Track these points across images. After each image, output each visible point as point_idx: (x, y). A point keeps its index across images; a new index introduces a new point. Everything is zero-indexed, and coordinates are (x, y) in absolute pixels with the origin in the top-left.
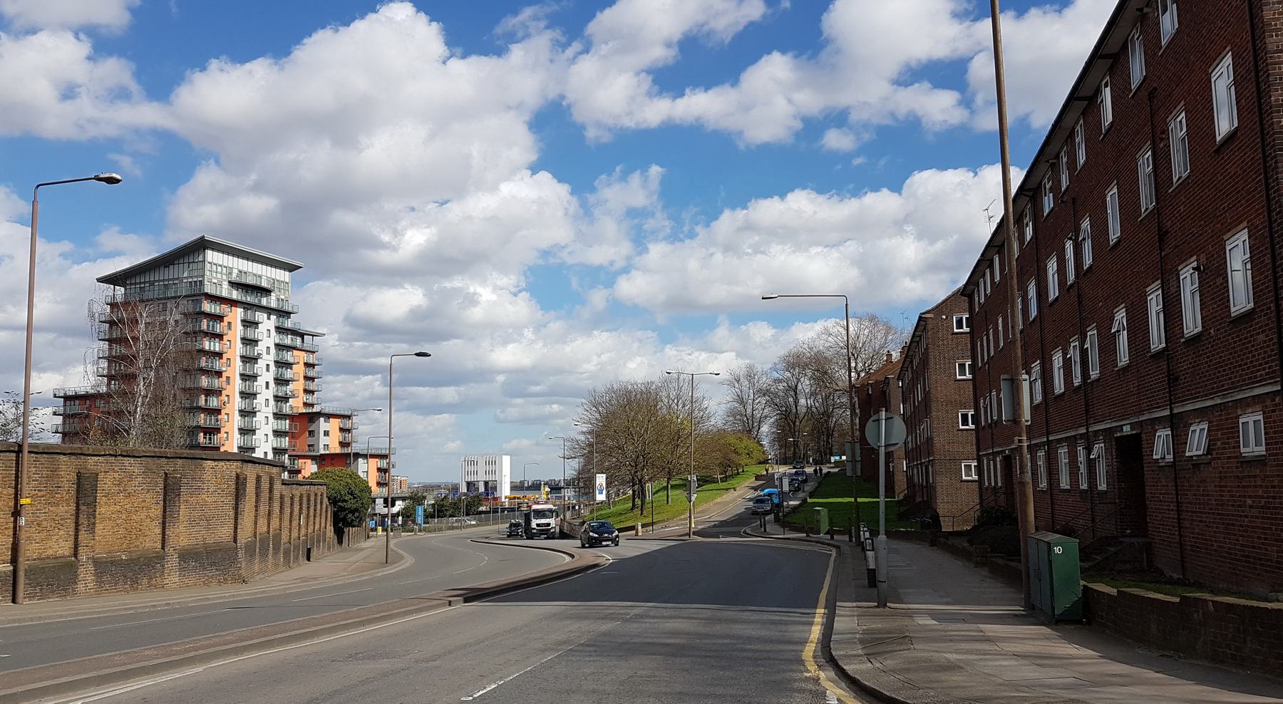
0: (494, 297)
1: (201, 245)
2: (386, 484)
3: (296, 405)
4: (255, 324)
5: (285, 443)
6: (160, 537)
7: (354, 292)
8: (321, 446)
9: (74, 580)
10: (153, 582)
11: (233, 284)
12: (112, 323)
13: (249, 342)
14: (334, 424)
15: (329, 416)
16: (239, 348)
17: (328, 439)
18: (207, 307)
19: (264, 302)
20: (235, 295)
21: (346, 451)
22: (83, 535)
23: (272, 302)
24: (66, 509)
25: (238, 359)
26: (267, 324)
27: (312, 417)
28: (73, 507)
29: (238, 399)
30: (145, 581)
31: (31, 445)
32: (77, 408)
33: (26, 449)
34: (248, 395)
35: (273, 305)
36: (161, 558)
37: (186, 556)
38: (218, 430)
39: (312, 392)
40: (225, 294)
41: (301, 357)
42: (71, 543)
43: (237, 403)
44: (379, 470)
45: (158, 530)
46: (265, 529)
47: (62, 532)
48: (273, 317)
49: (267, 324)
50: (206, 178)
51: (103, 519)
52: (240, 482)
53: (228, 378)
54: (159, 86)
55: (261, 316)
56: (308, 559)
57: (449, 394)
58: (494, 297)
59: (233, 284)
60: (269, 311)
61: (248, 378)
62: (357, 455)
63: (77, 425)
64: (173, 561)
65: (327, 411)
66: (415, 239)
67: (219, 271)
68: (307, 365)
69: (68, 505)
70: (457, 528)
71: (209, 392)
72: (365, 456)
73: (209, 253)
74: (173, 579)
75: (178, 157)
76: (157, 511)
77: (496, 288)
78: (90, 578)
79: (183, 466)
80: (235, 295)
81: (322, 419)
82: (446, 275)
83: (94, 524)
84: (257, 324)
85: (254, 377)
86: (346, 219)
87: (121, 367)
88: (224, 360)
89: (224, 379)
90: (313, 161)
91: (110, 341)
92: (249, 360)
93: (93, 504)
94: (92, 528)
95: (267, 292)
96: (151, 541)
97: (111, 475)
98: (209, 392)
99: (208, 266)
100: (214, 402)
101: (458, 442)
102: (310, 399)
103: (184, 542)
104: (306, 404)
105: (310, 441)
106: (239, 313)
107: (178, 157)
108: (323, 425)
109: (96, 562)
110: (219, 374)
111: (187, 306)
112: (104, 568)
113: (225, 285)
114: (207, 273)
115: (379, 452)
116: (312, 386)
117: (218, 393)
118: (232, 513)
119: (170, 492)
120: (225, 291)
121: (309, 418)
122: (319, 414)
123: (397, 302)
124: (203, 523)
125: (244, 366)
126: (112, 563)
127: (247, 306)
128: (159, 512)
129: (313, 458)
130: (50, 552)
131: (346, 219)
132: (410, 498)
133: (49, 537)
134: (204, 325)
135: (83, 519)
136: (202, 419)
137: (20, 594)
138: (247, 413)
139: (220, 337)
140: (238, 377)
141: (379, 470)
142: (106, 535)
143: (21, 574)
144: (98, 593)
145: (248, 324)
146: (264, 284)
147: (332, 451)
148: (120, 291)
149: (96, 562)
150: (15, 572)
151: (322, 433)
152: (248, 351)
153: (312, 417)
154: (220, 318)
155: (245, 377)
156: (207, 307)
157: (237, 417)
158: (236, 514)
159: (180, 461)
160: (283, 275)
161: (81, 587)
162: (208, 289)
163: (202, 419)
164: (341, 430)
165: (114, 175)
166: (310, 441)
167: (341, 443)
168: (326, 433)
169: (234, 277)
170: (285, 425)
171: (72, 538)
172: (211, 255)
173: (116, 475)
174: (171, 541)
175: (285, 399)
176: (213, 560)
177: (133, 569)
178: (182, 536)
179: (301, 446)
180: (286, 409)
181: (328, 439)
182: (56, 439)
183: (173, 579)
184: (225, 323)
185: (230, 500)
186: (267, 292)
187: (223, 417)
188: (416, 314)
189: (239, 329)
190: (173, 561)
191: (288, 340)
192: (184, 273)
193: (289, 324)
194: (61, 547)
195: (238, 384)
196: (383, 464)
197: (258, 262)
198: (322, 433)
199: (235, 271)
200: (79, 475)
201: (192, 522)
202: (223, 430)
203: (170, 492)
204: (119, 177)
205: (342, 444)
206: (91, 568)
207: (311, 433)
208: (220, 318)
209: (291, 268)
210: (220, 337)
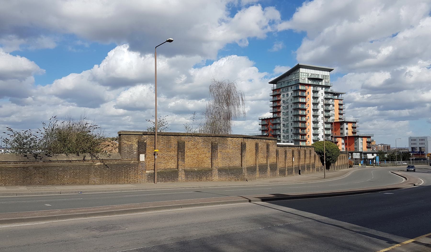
0: (420, 71)
1: (298, 67)
2: (370, 148)
3: (335, 118)
4: (317, 92)
5: (330, 132)
6: (211, 163)
7: (363, 76)
8: (345, 133)
9: (177, 176)
10: (208, 178)
11: (309, 79)
12: (273, 96)
13: (315, 98)
14: (350, 126)
15: (347, 123)
16: (312, 100)
17: (348, 131)
18: (301, 87)
19: (320, 83)
20: (310, 82)
21: (355, 135)
22: (180, 162)
23: (323, 83)
24: (174, 153)
25: (312, 104)
26: (321, 92)
27: (342, 123)
28: (176, 153)
29: (312, 117)
30: (205, 178)
31: (158, 133)
32: (265, 123)
33: (156, 134)
34: (315, 116)
35: (324, 84)
36: (211, 170)
37: (221, 170)
38: (306, 128)
39: (342, 114)
40: (306, 82)
41: (336, 103)
42: (176, 164)
43: (312, 119)
44: (367, 142)
45: (210, 161)
46: (313, 162)
47: (173, 161)
48: (324, 89)
49: (321, 92)
50: (306, 44)
51: (188, 157)
52: (257, 145)
53: (308, 111)
54: (287, 15)
55: (319, 89)
56: (300, 174)
57: (405, 112)
58: (420, 71)
59: (309, 79)
60: (322, 86)
61: (315, 110)
62: (358, 137)
63: (266, 128)
64: (215, 172)
65: (347, 121)
66: (386, 51)
67: (304, 75)
68: (340, 105)
69: (175, 152)
70: (398, 165)
71: (302, 116)
72: (362, 137)
73: (301, 69)
74: (216, 177)
75: (294, 38)
76: (209, 155)
77: (422, 67)
78: (183, 176)
79: (219, 139)
80: (310, 82)
81: (345, 124)
82: (399, 65)
83: (184, 158)
84: (318, 91)
85: (317, 110)
86: (359, 49)
87: (276, 109)
88: (307, 105)
89: (307, 111)
90: (340, 29)
91: (273, 101)
92: (315, 104)
93: (183, 152)
94: (183, 160)
95: (321, 80)
96: (207, 164)
97: (190, 142)
98: (302, 116)
99: (300, 74)
100: (304, 119)
101: (411, 132)
102: (341, 117)
103: (220, 165)
104: (339, 119)
105: (341, 131)
106: (312, 88)
107: (294, 38)
108: (345, 126)
109: (185, 171)
110: (305, 110)
111: (294, 88)
112: (189, 173)
113: (307, 79)
114: (300, 76)
115: (367, 135)
116: (342, 112)
117: (305, 116)
118: (240, 156)
119: (214, 148)
120: (307, 81)
121: (340, 124)
122: (344, 122)
123: (380, 78)
124: (229, 159)
125: (314, 106)
126: (192, 171)
127: (314, 86)
128: (210, 155)
129: (342, 138)
130: (168, 167)
131: (359, 49)
132: (378, 153)
133: (168, 162)
134: (300, 94)
135: (180, 157)
136: (300, 125)
137: (156, 180)
138: (315, 122)
139: (305, 97)
140: (312, 110)
141: (367, 142)
142: (190, 161)
143: (156, 174)
144: (186, 181)
145: (314, 92)
146: (320, 77)
147: (349, 135)
148: (275, 85)
149: (185, 171)
150: (154, 173)
151: (345, 129)
152: (315, 101)
153: (342, 123)
154: (305, 91)
155: (314, 110)
156: (301, 87)
157: (312, 124)
158: (242, 156)
159: (218, 138)
160: (327, 73)
161: (180, 179)
162: (301, 81)
163: (300, 125)
164: (352, 127)
165: (170, 39)
166: (341, 131)
167: (352, 132)
168: (347, 129)
169: (309, 76)
170: (329, 126)
171: (177, 163)
172: (301, 70)
173: (193, 142)
174: (215, 165)
175: (329, 117)
176: (233, 172)
177: (202, 173)
178: (220, 163)
179: (338, 134)
180: (330, 120)
181: (348, 131)
182: (260, 133)
183: (216, 177)
184: (307, 92)
185: (239, 151)
186: (321, 80)
187: (307, 124)
188: (388, 82)
189: (311, 94)
190: (215, 172)
191: (330, 96)
192: (293, 77)
193: (329, 90)
194: (172, 165)
195: (312, 113)
196: (369, 140)
197: (318, 70)
198: (345, 129)
199: (310, 74)
200: (178, 142)
201: (223, 159)
202: (307, 128)
203: (214, 148)
204: (172, 39)
205: (353, 133)
206: (183, 172)
207: (342, 129)
208: (305, 91)
209: (330, 70)
210: (305, 97)
